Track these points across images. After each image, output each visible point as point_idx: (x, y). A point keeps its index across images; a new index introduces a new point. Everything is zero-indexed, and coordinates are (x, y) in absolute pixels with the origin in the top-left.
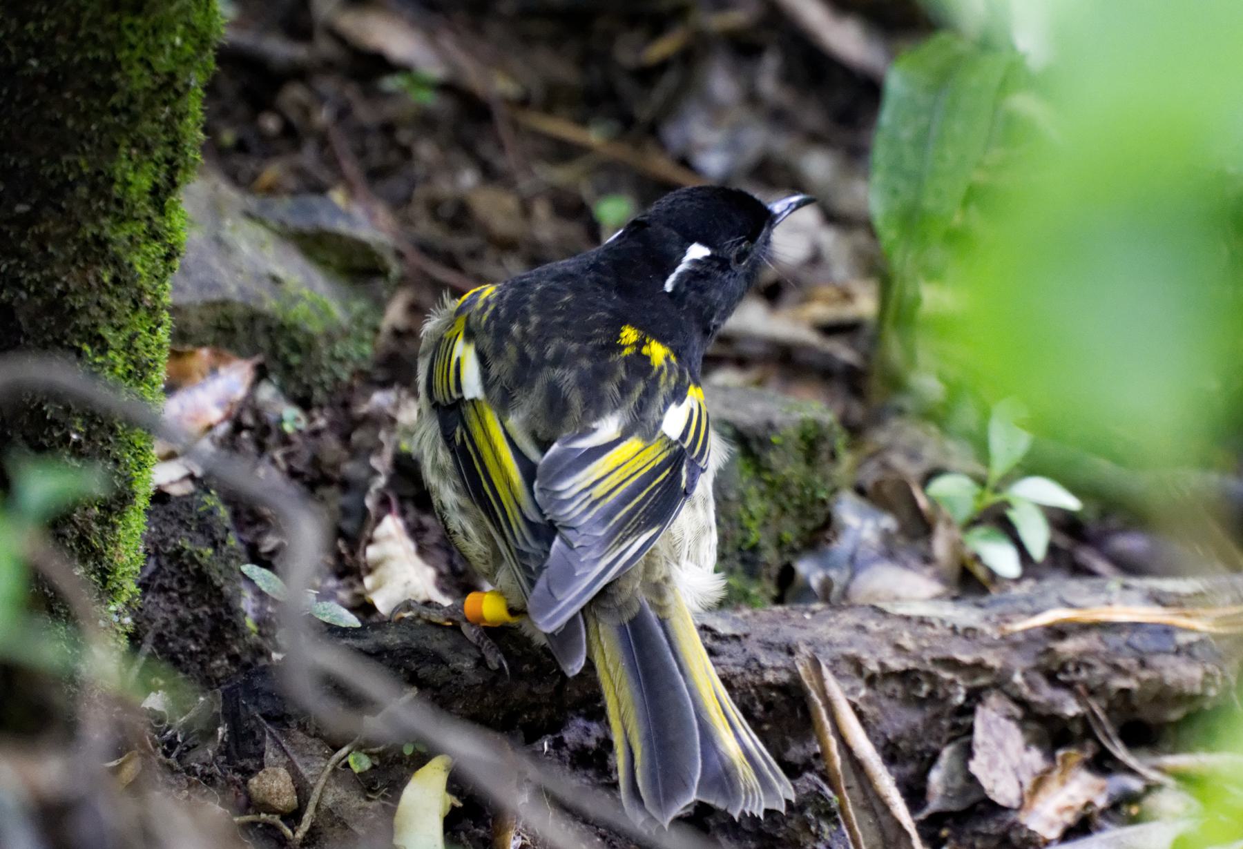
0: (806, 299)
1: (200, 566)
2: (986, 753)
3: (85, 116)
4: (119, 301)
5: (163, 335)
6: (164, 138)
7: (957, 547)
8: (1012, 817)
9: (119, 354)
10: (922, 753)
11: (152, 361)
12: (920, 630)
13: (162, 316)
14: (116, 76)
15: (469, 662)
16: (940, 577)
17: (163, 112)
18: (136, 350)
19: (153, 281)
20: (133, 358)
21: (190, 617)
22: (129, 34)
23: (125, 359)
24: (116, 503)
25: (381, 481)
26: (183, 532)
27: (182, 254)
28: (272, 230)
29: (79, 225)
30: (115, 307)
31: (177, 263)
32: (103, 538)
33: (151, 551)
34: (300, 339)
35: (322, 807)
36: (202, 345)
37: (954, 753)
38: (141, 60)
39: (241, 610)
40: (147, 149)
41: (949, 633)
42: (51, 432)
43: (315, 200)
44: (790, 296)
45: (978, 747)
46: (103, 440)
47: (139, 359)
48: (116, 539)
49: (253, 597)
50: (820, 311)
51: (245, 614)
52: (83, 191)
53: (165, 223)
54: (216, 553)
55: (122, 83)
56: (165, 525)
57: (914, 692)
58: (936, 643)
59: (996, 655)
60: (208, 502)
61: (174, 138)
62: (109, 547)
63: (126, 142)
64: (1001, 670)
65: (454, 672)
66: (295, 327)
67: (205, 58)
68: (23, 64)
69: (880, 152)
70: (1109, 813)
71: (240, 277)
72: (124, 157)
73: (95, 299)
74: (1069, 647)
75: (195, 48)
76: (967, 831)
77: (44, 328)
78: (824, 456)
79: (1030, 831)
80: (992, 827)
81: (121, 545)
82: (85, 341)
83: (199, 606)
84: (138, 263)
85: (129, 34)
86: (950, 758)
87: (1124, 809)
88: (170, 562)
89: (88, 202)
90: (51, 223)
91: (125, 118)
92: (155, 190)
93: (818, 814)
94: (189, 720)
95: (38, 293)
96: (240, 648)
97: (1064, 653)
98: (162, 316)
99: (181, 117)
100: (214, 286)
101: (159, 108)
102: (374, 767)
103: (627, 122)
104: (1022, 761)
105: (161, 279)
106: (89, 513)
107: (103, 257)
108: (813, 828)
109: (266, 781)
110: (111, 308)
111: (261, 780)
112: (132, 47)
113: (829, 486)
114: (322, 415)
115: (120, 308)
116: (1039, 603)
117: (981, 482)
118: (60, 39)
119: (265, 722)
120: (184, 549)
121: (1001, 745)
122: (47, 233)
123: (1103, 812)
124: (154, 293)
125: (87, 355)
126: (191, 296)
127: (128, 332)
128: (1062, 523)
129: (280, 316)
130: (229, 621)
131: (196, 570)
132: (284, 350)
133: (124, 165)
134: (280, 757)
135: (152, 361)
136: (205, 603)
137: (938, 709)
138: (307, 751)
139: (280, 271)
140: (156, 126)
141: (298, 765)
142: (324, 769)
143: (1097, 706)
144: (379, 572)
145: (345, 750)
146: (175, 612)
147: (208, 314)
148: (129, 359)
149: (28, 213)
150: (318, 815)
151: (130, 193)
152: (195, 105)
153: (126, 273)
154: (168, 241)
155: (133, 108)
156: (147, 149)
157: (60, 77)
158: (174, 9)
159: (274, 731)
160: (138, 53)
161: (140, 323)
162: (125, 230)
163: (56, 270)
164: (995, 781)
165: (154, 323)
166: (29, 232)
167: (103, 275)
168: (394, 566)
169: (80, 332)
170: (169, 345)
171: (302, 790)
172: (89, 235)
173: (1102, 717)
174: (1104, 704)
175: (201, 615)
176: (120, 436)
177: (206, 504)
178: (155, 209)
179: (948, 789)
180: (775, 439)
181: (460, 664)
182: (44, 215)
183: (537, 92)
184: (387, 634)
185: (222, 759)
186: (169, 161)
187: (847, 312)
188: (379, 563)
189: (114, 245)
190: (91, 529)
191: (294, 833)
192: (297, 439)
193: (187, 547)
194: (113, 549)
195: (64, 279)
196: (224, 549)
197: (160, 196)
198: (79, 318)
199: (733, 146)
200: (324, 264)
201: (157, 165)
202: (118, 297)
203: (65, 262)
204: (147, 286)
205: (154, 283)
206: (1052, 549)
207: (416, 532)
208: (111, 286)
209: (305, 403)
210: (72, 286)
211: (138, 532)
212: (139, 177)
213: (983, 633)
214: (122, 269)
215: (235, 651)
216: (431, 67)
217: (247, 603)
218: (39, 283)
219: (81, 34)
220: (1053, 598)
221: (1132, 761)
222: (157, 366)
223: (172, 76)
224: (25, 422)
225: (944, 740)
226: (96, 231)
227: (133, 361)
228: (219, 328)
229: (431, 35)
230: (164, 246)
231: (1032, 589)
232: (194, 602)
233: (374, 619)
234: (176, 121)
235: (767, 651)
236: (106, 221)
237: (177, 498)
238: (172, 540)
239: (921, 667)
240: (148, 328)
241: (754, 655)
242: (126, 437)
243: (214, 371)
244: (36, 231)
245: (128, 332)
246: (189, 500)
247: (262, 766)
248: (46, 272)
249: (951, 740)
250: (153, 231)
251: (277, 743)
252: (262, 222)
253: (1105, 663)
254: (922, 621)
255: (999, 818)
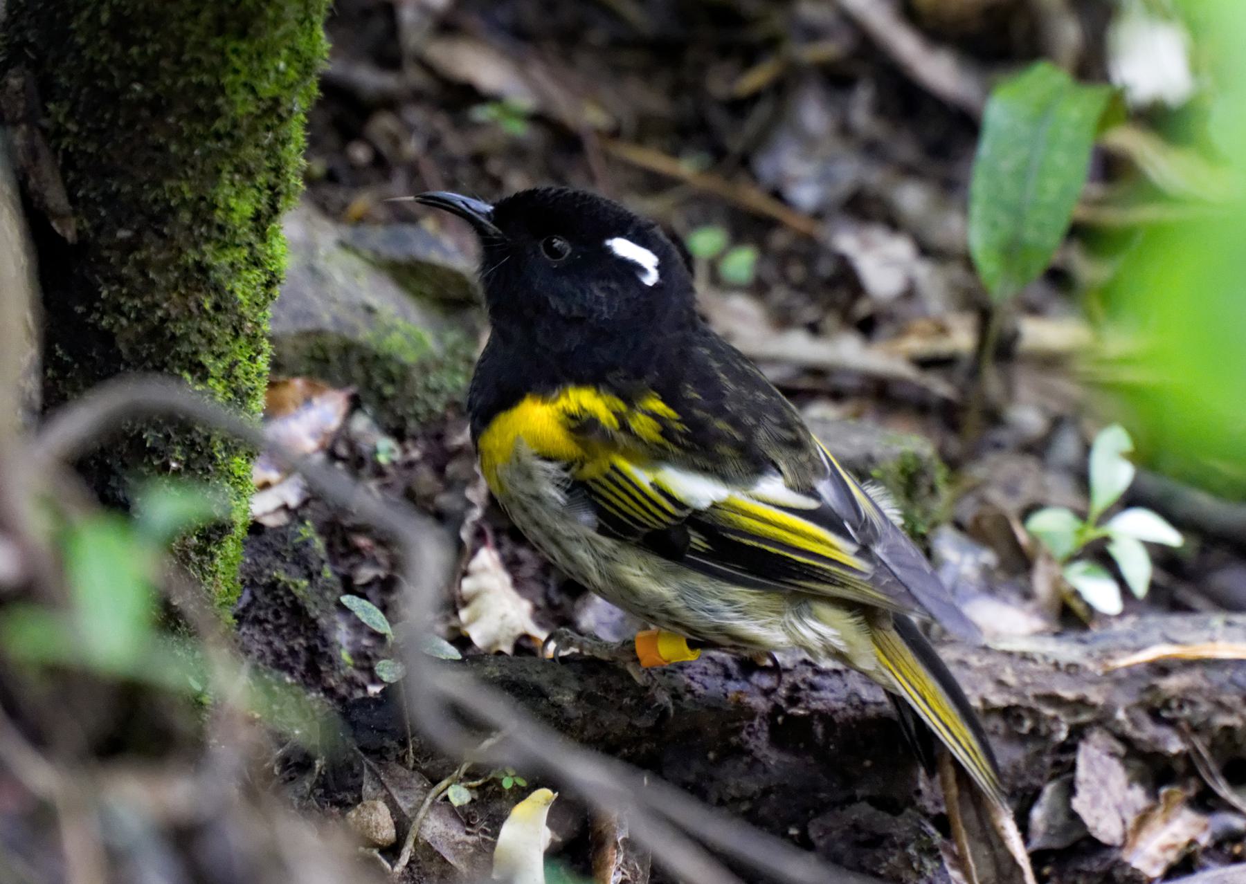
0: (902, 332)
1: (296, 598)
2: (1089, 791)
3: (189, 142)
4: (220, 328)
5: (263, 363)
6: (267, 164)
7: (1057, 582)
8: (1115, 855)
9: (219, 382)
10: (1024, 790)
11: (252, 390)
12: (1022, 666)
13: (261, 344)
14: (220, 101)
15: (569, 695)
16: (1040, 612)
17: (266, 138)
18: (236, 378)
19: (253, 308)
20: (233, 385)
21: (285, 649)
22: (233, 58)
23: (225, 387)
24: (215, 533)
25: (477, 513)
26: (278, 563)
27: (282, 281)
28: (367, 260)
29: (180, 251)
30: (216, 335)
31: (277, 291)
32: (201, 568)
33: (247, 582)
34: (394, 369)
35: (420, 841)
36: (295, 375)
37: (1057, 790)
38: (245, 85)
39: (337, 642)
40: (250, 175)
41: (1051, 669)
42: (150, 461)
43: (408, 230)
44: (885, 330)
45: (1080, 783)
46: (202, 469)
47: (239, 387)
48: (213, 569)
49: (347, 629)
50: (916, 344)
51: (341, 647)
52: (185, 217)
53: (266, 249)
54: (311, 585)
55: (226, 108)
56: (259, 557)
57: (1016, 728)
58: (1039, 679)
59: (1099, 692)
60: (304, 534)
61: (276, 164)
62: (207, 576)
63: (229, 167)
64: (1104, 706)
65: (554, 705)
66: (389, 358)
67: (308, 83)
68: (126, 88)
69: (979, 184)
70: (1212, 852)
71: (334, 308)
72: (227, 182)
73: (196, 326)
74: (1172, 684)
75: (298, 72)
76: (1070, 869)
77: (144, 355)
78: (924, 490)
79: (1133, 869)
80: (1095, 865)
81: (219, 575)
82: (185, 368)
83: (295, 637)
84: (239, 290)
85: (233, 58)
86: (1053, 794)
87: (1227, 848)
88: (266, 593)
89: (190, 228)
90: (152, 249)
91: (228, 143)
92: (257, 217)
93: (920, 851)
94: (286, 753)
95: (139, 319)
96: (336, 682)
97: (1167, 690)
98: (261, 344)
99: (284, 143)
100: (309, 315)
101: (262, 133)
102: (473, 801)
103: (719, 154)
104: (1125, 798)
105: (260, 306)
106: (187, 543)
107: (204, 283)
108: (915, 865)
109: (365, 814)
110: (211, 335)
111: (359, 813)
112: (236, 72)
113: (929, 521)
114: (416, 446)
115: (220, 334)
116: (1142, 639)
117: (1082, 516)
118: (164, 63)
119: (363, 755)
120: (279, 581)
121: (1103, 782)
122: (148, 259)
123: (1206, 851)
124: (255, 320)
125: (187, 383)
126: (287, 327)
127: (228, 360)
128: (1162, 557)
129: (374, 346)
130: (325, 653)
131: (291, 602)
132: (378, 381)
133: (227, 190)
134: (379, 790)
135: (252, 390)
136: (300, 635)
137: (1039, 746)
138: (405, 784)
139: (374, 301)
140: (259, 151)
141: (396, 798)
142: (423, 802)
143: (1200, 744)
144: (475, 605)
145: (444, 783)
146: (270, 644)
147: (303, 344)
148: (229, 387)
149: (129, 239)
150: (416, 850)
151: (232, 218)
152: (297, 133)
153: (227, 300)
154: (269, 268)
155: (236, 133)
156: (250, 175)
157: (163, 102)
158: (278, 33)
159: (372, 763)
160: (243, 78)
161: (240, 351)
162: (227, 256)
163: (158, 297)
164: (1097, 819)
165: (254, 351)
166: (131, 257)
167: (204, 301)
168: (489, 598)
169: (180, 360)
170: (268, 374)
171: (402, 825)
172: (190, 261)
173: (1205, 754)
174: (1207, 741)
175: (297, 647)
176: (219, 465)
177: (301, 535)
178: (257, 235)
179: (1050, 827)
180: (875, 473)
181: (560, 697)
182: (146, 240)
183: (629, 124)
184: (486, 666)
185: (319, 792)
186: (271, 188)
187: (944, 346)
188: (475, 596)
189: (216, 271)
190: (190, 559)
191: (393, 867)
192: (390, 470)
193: (283, 578)
194: (211, 579)
195: (165, 305)
196: (320, 581)
197: (262, 222)
198: (179, 346)
199: (826, 178)
200: (418, 294)
201: (260, 191)
202: (219, 324)
203: (167, 289)
204: (247, 313)
205: (255, 310)
206: (1153, 587)
207: (511, 564)
208: (212, 312)
209: (399, 434)
210: (174, 313)
211: (235, 562)
212: (241, 203)
213: (1086, 670)
214: (224, 296)
215: (330, 684)
216: (523, 100)
217: (342, 635)
218: (140, 310)
219: (186, 58)
220: (1156, 633)
221: (1235, 799)
222: (256, 394)
223: (276, 101)
224: (125, 450)
225: (1047, 776)
226: (197, 258)
227: (232, 389)
228: (313, 358)
229: (520, 65)
230: (265, 273)
231: (1134, 624)
232: (289, 634)
233: (470, 652)
234: (279, 147)
235: (869, 686)
236: (208, 248)
237: (272, 529)
238: (267, 571)
239: (1024, 703)
240: (248, 355)
241: (856, 689)
242: (225, 466)
243: (308, 401)
244: (138, 257)
245: (228, 360)
246: (283, 531)
247: (360, 800)
248: (147, 299)
249: (1053, 777)
250: (254, 258)
251: (375, 776)
252: (356, 252)
253: (1209, 700)
254: (1025, 657)
255: (1103, 856)
